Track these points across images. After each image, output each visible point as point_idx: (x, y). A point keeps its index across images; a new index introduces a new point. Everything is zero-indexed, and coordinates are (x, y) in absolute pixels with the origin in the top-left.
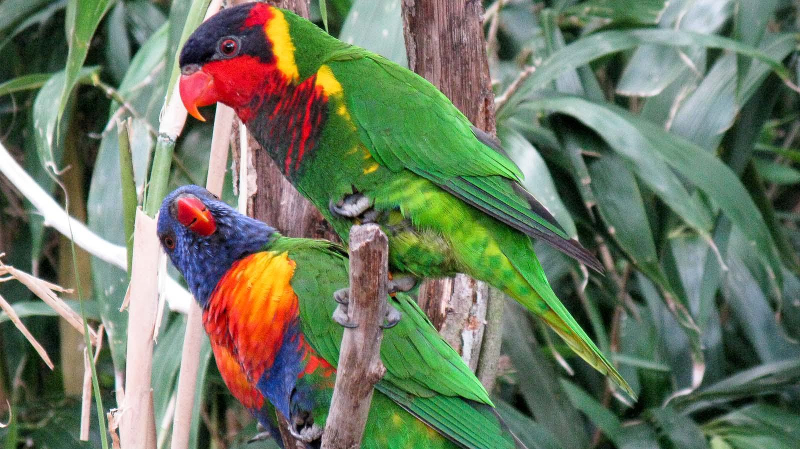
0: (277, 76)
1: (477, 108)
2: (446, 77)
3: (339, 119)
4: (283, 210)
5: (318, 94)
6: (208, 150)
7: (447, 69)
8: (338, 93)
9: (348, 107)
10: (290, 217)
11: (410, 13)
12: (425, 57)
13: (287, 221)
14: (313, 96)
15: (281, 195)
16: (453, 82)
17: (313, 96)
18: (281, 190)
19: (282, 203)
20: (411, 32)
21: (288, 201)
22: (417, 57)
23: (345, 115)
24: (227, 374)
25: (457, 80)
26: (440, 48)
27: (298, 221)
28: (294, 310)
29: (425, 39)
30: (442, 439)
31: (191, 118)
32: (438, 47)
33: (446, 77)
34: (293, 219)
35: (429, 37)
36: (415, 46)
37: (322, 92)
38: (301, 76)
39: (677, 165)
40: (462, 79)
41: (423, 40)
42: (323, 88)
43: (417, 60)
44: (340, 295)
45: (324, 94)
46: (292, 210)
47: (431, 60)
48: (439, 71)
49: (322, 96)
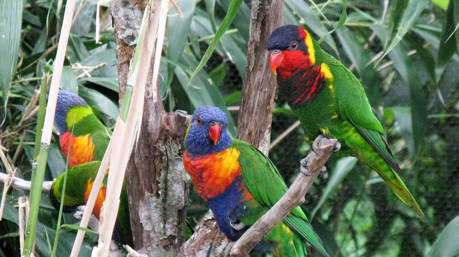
0: (308, 61)
1: (274, 89)
2: (266, 74)
3: (329, 90)
4: (150, 124)
5: (322, 76)
6: (433, 108)
7: (267, 70)
9: (334, 86)
10: (153, 127)
13: (152, 129)
14: (319, 75)
15: (149, 117)
16: (268, 76)
18: (149, 115)
19: (149, 121)
21: (152, 120)
22: (255, 64)
23: (332, 89)
24: (449, 218)
27: (156, 129)
28: (239, 172)
32: (266, 61)
33: (266, 74)
34: (154, 128)
35: (264, 56)
36: (255, 59)
37: (324, 75)
38: (316, 64)
39: (14, 91)
40: (272, 75)
42: (324, 74)
44: (303, 162)
45: (325, 76)
46: (154, 124)
47: (262, 66)
48: (264, 71)
49: (323, 77)
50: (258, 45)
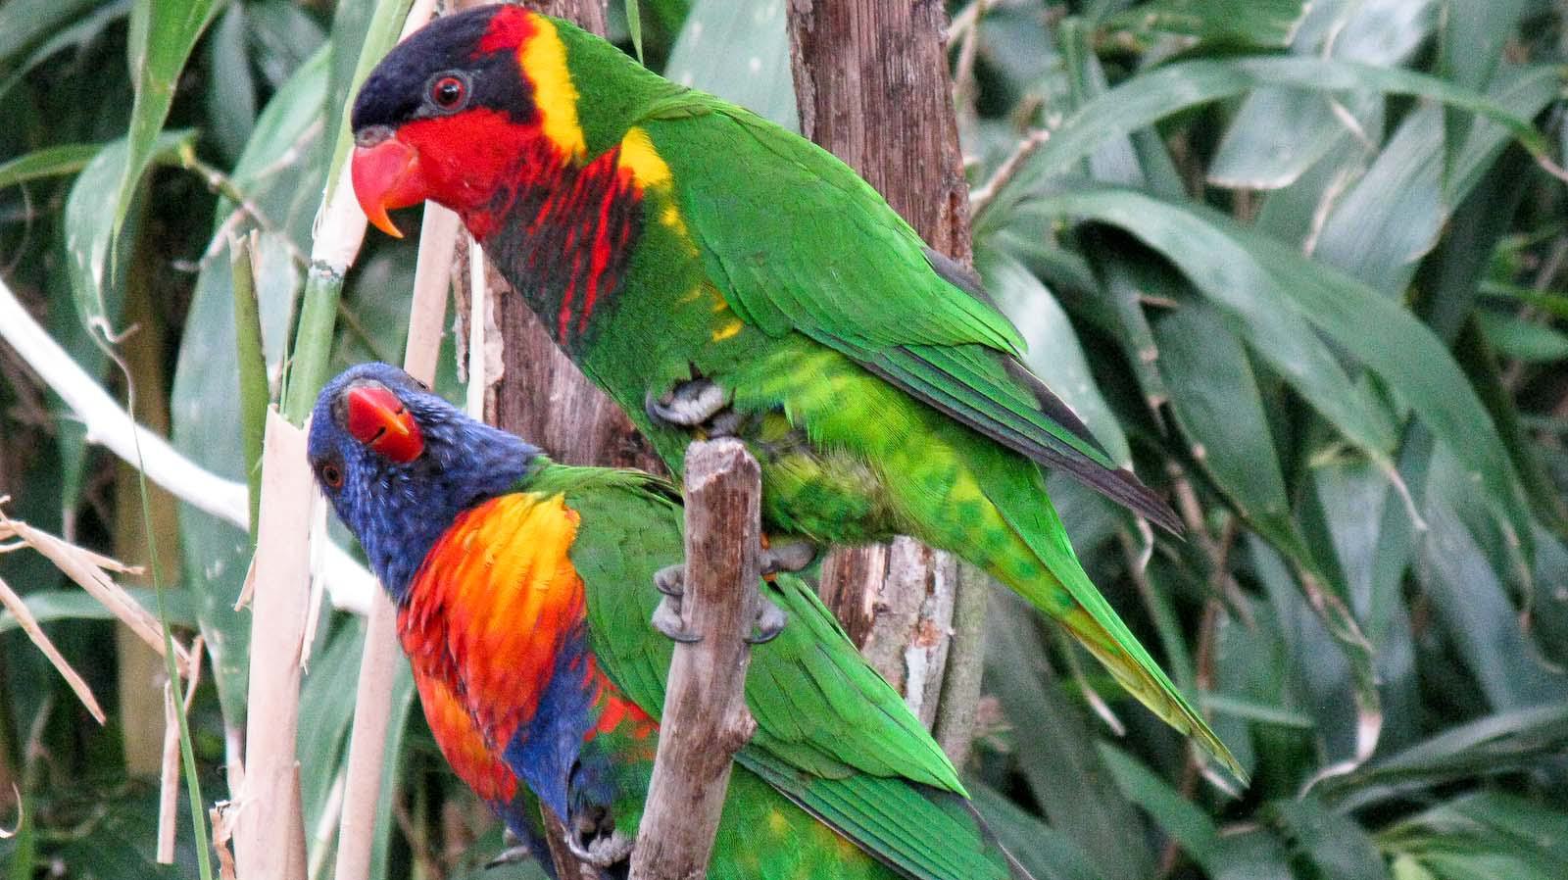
0: (544, 149)
1: (935, 213)
2: (875, 151)
3: (665, 232)
4: (555, 411)
5: (624, 183)
6: (407, 294)
7: (876, 136)
8: (662, 182)
9: (683, 210)
10: (568, 426)
11: (804, 25)
12: (834, 112)
13: (563, 433)
14: (613, 188)
15: (550, 383)
16: (888, 162)
17: (613, 188)
18: (551, 373)
19: (552, 399)
20: (805, 63)
21: (565, 395)
22: (817, 111)
23: (677, 225)
24: (446, 732)
25: (897, 156)
26: (862, 94)
27: (584, 433)
28: (575, 608)
29: (833, 77)
30: (867, 859)
31: (374, 231)
32: (858, 93)
33: (875, 151)
34: (574, 430)
35: (841, 72)
36: (814, 90)
37: (632, 180)
38: (589, 148)
39: (1326, 323)
40: (905, 155)
41: (830, 78)
42: (632, 173)
43: (818, 117)
44: (665, 577)
45: (635, 184)
46: (573, 411)
47: (844, 118)
48: (861, 139)
49: (631, 188)
50: (811, 28)
